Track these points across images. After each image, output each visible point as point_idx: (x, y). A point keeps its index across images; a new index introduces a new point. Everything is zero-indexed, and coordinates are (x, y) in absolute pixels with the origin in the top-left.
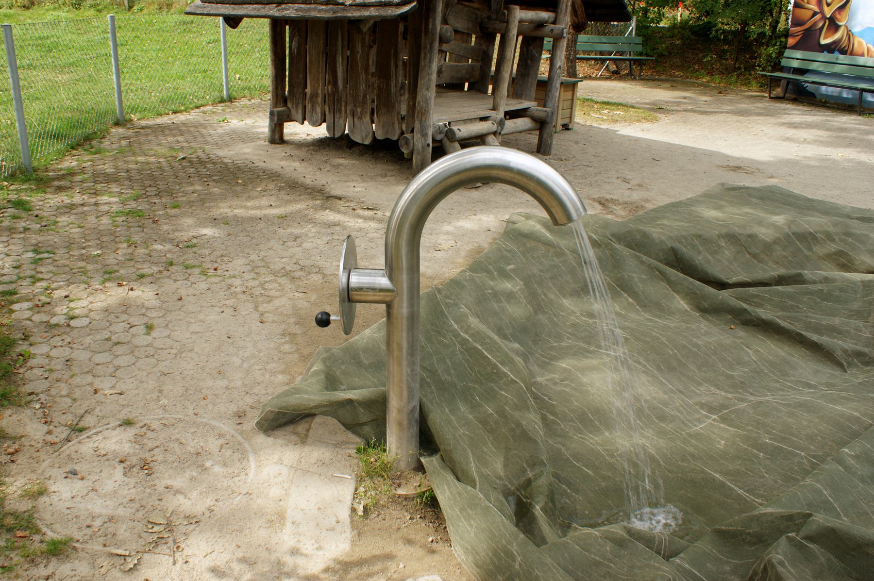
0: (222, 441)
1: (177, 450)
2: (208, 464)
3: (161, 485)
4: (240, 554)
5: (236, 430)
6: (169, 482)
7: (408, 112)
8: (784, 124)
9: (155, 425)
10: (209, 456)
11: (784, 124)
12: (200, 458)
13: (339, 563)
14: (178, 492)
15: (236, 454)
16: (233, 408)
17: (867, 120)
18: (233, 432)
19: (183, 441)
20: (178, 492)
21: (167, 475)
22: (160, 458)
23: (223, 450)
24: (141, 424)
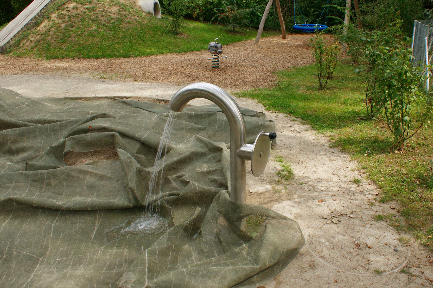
0: (322, 254)
1: (344, 253)
2: (327, 243)
3: (347, 237)
4: (312, 209)
5: (314, 257)
6: (344, 238)
7: (192, 110)
8: (22, 126)
9: (361, 270)
10: (327, 247)
11: (22, 126)
12: (332, 247)
13: (278, 202)
14: (339, 233)
15: (314, 246)
16: (317, 272)
17: (58, 96)
18: (317, 257)
19: (343, 257)
20: (339, 233)
21: (346, 241)
22: (352, 250)
23: (321, 249)
24: (370, 271)
